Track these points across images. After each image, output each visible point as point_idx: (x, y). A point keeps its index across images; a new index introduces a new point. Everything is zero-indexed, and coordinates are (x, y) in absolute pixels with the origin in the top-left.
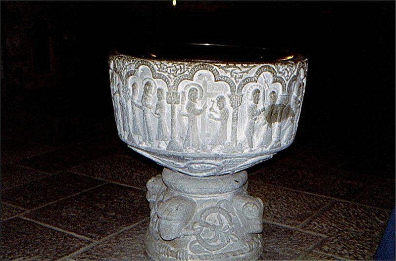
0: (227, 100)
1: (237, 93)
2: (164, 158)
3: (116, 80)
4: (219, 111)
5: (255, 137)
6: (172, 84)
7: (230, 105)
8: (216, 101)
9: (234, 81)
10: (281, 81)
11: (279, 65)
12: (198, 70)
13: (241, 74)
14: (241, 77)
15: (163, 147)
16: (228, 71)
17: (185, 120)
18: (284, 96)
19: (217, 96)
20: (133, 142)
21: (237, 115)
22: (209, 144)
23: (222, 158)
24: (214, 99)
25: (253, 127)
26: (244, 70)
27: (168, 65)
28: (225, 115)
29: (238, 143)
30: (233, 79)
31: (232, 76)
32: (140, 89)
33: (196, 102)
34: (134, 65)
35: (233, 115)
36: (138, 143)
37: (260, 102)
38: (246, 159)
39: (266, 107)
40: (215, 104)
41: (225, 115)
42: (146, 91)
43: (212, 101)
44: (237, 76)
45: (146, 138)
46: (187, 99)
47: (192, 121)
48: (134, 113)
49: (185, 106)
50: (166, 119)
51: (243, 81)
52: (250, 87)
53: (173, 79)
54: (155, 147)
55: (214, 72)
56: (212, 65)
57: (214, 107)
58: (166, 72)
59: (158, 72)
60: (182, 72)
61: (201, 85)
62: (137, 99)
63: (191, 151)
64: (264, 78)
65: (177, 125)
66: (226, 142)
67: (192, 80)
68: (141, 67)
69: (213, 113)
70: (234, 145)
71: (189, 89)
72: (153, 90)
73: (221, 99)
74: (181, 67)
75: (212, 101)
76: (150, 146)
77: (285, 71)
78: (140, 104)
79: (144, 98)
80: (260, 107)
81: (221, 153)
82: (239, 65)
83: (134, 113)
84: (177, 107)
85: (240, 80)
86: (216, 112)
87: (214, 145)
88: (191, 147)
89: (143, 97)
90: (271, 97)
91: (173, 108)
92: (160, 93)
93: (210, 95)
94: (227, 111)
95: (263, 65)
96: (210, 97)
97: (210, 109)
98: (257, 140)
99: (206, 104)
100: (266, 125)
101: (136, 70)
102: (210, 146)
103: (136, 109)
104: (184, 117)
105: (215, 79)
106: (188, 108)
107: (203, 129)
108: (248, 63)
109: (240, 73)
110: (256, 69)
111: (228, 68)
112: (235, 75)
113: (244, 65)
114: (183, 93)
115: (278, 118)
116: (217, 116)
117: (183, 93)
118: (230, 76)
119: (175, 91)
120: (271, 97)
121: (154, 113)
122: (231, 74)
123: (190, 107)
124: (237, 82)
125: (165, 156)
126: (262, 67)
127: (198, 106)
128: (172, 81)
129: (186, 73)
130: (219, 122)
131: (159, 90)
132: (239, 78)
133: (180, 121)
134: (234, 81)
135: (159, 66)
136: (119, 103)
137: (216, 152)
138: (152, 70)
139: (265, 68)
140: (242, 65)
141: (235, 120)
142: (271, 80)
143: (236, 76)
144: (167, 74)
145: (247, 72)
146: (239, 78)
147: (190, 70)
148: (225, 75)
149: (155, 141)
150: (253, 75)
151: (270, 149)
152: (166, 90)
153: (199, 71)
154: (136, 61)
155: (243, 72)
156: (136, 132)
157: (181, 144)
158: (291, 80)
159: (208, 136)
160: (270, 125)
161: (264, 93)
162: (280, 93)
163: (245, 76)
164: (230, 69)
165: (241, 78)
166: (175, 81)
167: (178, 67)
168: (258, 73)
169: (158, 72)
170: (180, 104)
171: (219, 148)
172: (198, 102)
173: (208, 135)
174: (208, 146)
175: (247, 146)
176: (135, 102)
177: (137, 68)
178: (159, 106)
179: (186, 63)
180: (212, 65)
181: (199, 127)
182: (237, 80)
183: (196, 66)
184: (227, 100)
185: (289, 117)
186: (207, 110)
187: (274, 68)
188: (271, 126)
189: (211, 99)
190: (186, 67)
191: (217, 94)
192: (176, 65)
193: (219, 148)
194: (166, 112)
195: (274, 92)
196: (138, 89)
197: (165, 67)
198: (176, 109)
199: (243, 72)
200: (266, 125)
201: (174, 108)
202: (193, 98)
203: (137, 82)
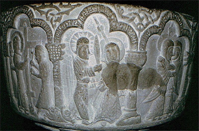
13: (59, 16)
26: (63, 10)
31: (47, 18)
38: (32, 71)
44: (54, 19)
51: (61, 25)
55: (29, 14)
77: (133, 15)
82: (57, 5)
85: (58, 24)
111: (43, 8)
112: (51, 17)
113: (63, 4)
118: (45, 19)
122: (46, 15)
125: (35, 67)
132: (56, 21)
134: (51, 26)
140: (61, 4)
145: (67, 13)
146: (56, 21)
150: (77, 18)
151: (118, 124)
155: (62, 13)
158: (147, 31)
163: (64, 18)
164: (46, 10)
168: (84, 16)
182: (54, 23)
199: (62, 13)
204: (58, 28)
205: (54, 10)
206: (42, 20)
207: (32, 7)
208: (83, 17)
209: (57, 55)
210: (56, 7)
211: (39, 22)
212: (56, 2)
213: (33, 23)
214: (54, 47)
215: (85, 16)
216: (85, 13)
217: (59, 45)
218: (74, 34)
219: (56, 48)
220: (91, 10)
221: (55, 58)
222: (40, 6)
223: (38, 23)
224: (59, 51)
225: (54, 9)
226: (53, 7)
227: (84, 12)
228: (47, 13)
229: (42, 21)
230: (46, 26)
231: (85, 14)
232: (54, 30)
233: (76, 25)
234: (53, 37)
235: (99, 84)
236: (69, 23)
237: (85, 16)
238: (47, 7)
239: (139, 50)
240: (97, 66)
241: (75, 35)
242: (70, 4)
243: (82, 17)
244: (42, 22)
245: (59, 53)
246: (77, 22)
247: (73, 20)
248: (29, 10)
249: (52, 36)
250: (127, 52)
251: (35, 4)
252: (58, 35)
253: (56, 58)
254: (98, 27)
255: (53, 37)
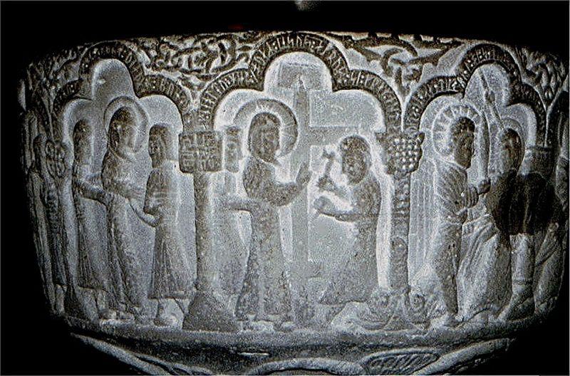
0: (375, 153)
1: (406, 127)
2: (177, 359)
3: (30, 129)
4: (349, 189)
5: (461, 279)
6: (194, 105)
7: (383, 167)
8: (338, 155)
9: (395, 88)
10: (532, 102)
11: (525, 52)
12: (279, 54)
13: (416, 67)
14: (416, 75)
15: (173, 318)
16: (375, 55)
17: (241, 223)
18: (542, 149)
19: (340, 140)
20: (82, 315)
21: (407, 200)
22: (321, 302)
23: (364, 349)
24: (333, 148)
25: (459, 240)
26: (423, 52)
27: (181, 47)
28: (370, 196)
29: (412, 293)
30: (392, 82)
31: (387, 71)
32: (95, 139)
33: (275, 161)
34: (76, 66)
35: (396, 201)
36: (96, 315)
37: (477, 160)
39: (494, 178)
40: (337, 166)
41: (370, 196)
42: (114, 137)
43: (325, 155)
44: (404, 72)
45: (117, 296)
46: (246, 152)
47: (264, 225)
48: (79, 218)
49: (238, 177)
50: (179, 225)
51: (422, 87)
52: (443, 113)
53: (200, 87)
54: (146, 325)
56: (324, 36)
57: (332, 175)
58: (177, 67)
59: (149, 71)
60: (226, 63)
61: (290, 104)
62: (87, 172)
63: (262, 328)
64: (485, 87)
65: (214, 241)
66: (375, 292)
67: (261, 89)
68: (98, 68)
69: (331, 196)
70: (401, 303)
71: (250, 118)
72: (138, 133)
73: (355, 147)
74: (221, 46)
75: (325, 155)
76: (131, 319)
78: (97, 187)
79: (109, 163)
80: (476, 177)
81: (360, 330)
82: (410, 39)
83: (79, 218)
84: (214, 180)
85: (414, 86)
86: (340, 193)
87: (336, 302)
88: (262, 311)
89: (104, 162)
90: (507, 147)
91: (200, 185)
92: (158, 137)
93: (319, 135)
94: (376, 188)
95: (479, 42)
96: (319, 142)
97: (323, 183)
98: (471, 291)
99: (306, 166)
100: (494, 238)
101: (84, 77)
102: (327, 308)
103: (88, 205)
104: (238, 214)
105: (334, 80)
106: (249, 182)
107: (300, 250)
108: (437, 33)
109: (412, 62)
110: (461, 52)
111: (374, 45)
112: (396, 67)
114: (233, 131)
115: (526, 219)
116: (345, 206)
117: (233, 131)
118: (380, 72)
119: (204, 128)
120: (507, 147)
121: (140, 210)
122: (384, 65)
123: (255, 178)
124: (404, 91)
126: (478, 47)
127: (283, 175)
128: (194, 97)
129: (242, 64)
130: (351, 225)
131: (156, 130)
133: (226, 224)
134: (395, 88)
135: (153, 53)
136: (38, 198)
137: (344, 327)
138: (134, 69)
139: (487, 50)
140: (417, 39)
141: (402, 215)
142: (505, 95)
143: (399, 72)
144: (180, 74)
145: (434, 60)
146: (410, 78)
147: (251, 53)
148: (365, 69)
149: (145, 300)
150: (452, 72)
151: (509, 317)
152: (176, 128)
153: (281, 57)
154: (82, 50)
155: (423, 60)
156: (87, 279)
157: (231, 307)
159: (319, 275)
160: (505, 241)
161: (486, 133)
162: (531, 139)
163: (428, 71)
164: (381, 49)
165: (417, 79)
166: (204, 95)
167: (212, 47)
168: (468, 66)
169: (149, 71)
170: (224, 171)
171: (353, 315)
172: (280, 160)
173: (318, 271)
174: (318, 306)
175: (441, 305)
176: (83, 180)
177: (88, 71)
178: (157, 184)
179: (241, 35)
180: (324, 36)
181: (287, 247)
182: (404, 84)
183: (271, 41)
184: (375, 153)
185: (551, 225)
186: (311, 187)
187: (512, 54)
188: (509, 246)
189: (321, 148)
190: (239, 45)
191: (341, 129)
192: (207, 41)
193: (353, 315)
194: (179, 200)
195: (512, 134)
196: (92, 138)
197: (173, 52)
198: (211, 189)
199: (423, 60)
200: (494, 238)
201: (206, 184)
202: (264, 149)
203: (88, 117)
204: (416, 94)
205: (401, 51)
206: (375, 75)
207: (340, 38)
208: (468, 71)
209: (411, 160)
210: (406, 45)
211: (364, 80)
212: (407, 32)
213: (345, 81)
214: (404, 140)
215: (471, 68)
216: (470, 63)
217: (416, 136)
218: (441, 111)
219: (410, 144)
220: (481, 57)
221: (404, 167)
222: (364, 40)
223: (361, 82)
224: (417, 150)
225: (402, 48)
226: (400, 45)
227: (469, 61)
228: (387, 56)
229: (372, 77)
230: (384, 89)
231: (472, 65)
232: (404, 101)
233: (454, 90)
234: (402, 116)
235: (482, 224)
236: (440, 85)
237: (471, 68)
238: (385, 43)
239: (546, 145)
240: (485, 181)
241: (445, 112)
242: (439, 41)
243: (465, 72)
244: (373, 80)
245: (416, 153)
246: (456, 83)
247: (448, 78)
248: (330, 46)
249: (400, 113)
250: (531, 148)
251: (349, 31)
252: (415, 112)
253: (407, 167)
254: (487, 95)
255: (402, 116)
